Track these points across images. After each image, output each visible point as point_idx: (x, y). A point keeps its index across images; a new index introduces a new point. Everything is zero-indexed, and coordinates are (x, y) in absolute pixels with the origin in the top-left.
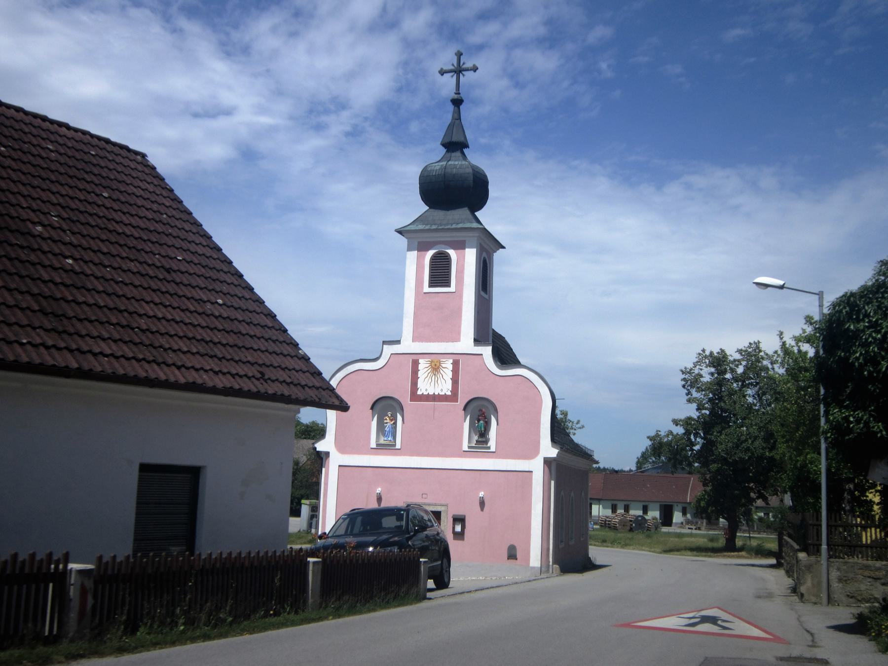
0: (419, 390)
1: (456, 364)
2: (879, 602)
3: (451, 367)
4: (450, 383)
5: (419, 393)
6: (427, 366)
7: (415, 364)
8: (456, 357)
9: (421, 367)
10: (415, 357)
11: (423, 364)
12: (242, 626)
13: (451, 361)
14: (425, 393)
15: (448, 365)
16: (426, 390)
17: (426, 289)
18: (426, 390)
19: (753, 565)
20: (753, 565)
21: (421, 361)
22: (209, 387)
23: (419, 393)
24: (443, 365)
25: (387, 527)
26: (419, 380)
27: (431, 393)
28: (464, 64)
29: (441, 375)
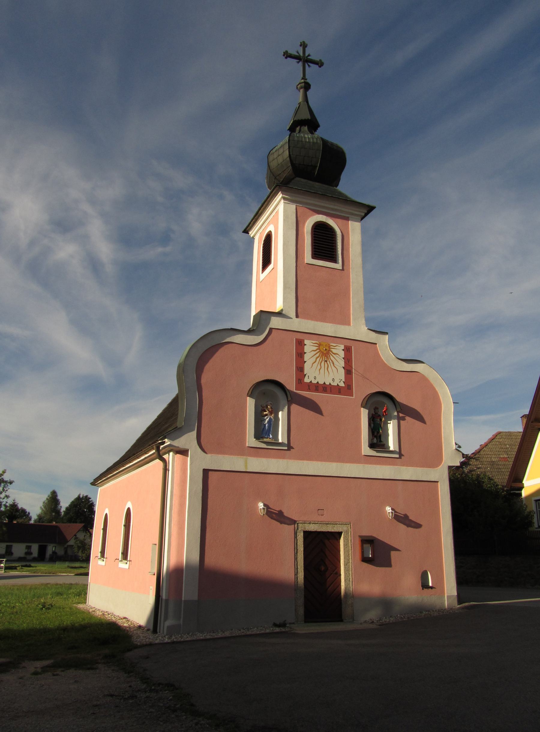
0: (306, 377)
1: (348, 350)
2: (106, 615)
3: (342, 354)
4: (342, 372)
5: (306, 380)
6: (315, 350)
7: (300, 344)
8: (348, 343)
9: (307, 349)
10: (300, 336)
11: (310, 346)
12: (78, 624)
13: (342, 347)
14: (314, 382)
15: (339, 350)
16: (315, 378)
17: (308, 257)
18: (315, 378)
19: (400, 513)
20: (400, 513)
21: (306, 342)
22: (57, 499)
23: (306, 380)
24: (334, 351)
25: (197, 594)
26: (306, 365)
27: (321, 382)
28: (309, 66)
29: (326, 365)
